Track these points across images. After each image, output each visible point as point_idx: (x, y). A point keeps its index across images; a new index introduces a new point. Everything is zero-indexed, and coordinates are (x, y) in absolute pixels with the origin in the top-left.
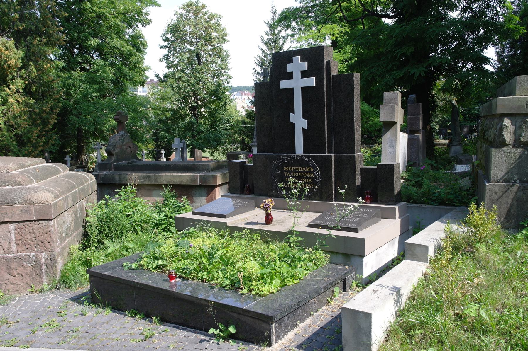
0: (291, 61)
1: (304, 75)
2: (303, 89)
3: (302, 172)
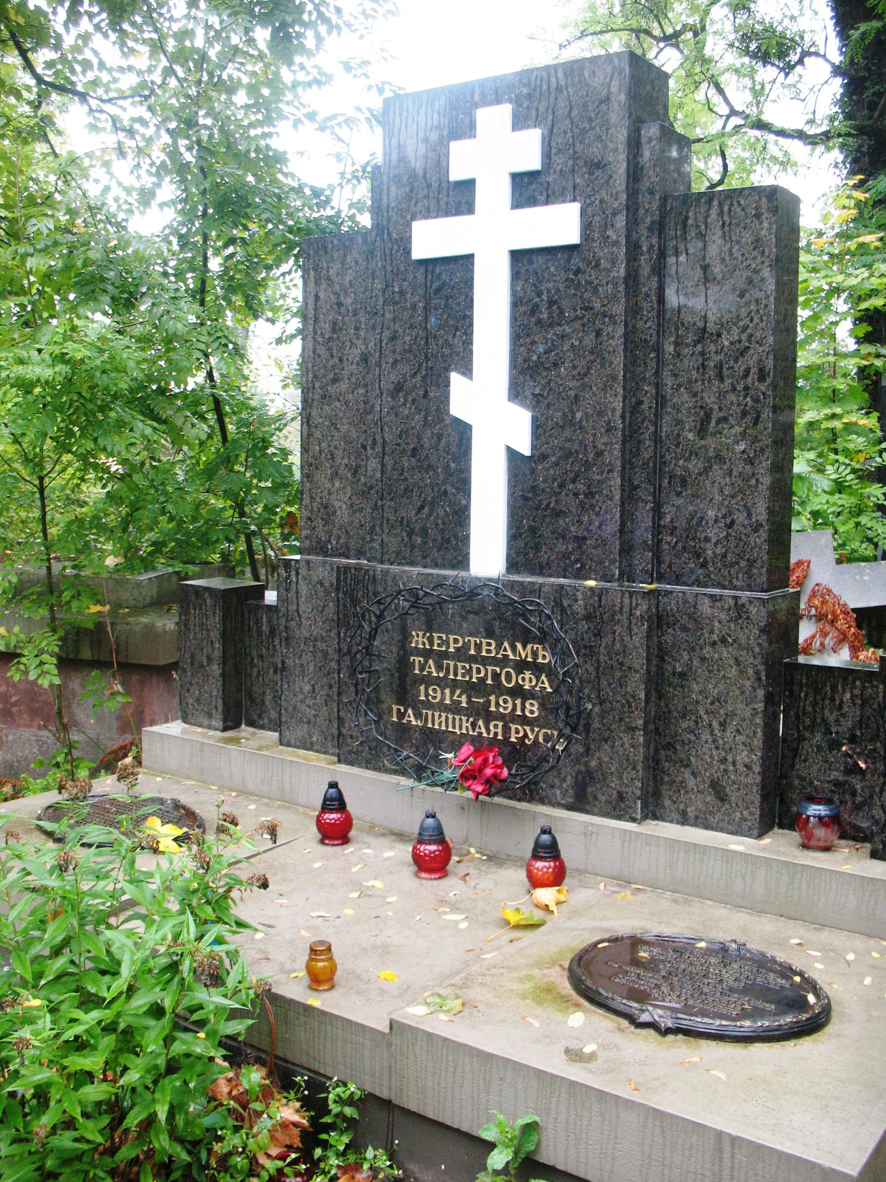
1: (528, 189)
3: (494, 661)
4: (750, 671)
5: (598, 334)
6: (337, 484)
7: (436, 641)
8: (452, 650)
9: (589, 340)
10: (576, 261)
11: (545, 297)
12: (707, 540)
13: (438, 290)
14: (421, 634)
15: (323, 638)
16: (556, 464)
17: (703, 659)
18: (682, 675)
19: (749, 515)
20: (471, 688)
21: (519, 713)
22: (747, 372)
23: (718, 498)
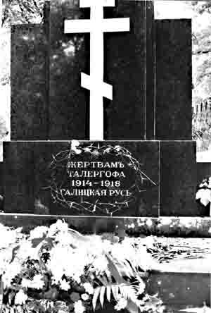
3: (102, 169)
20: (92, 180)
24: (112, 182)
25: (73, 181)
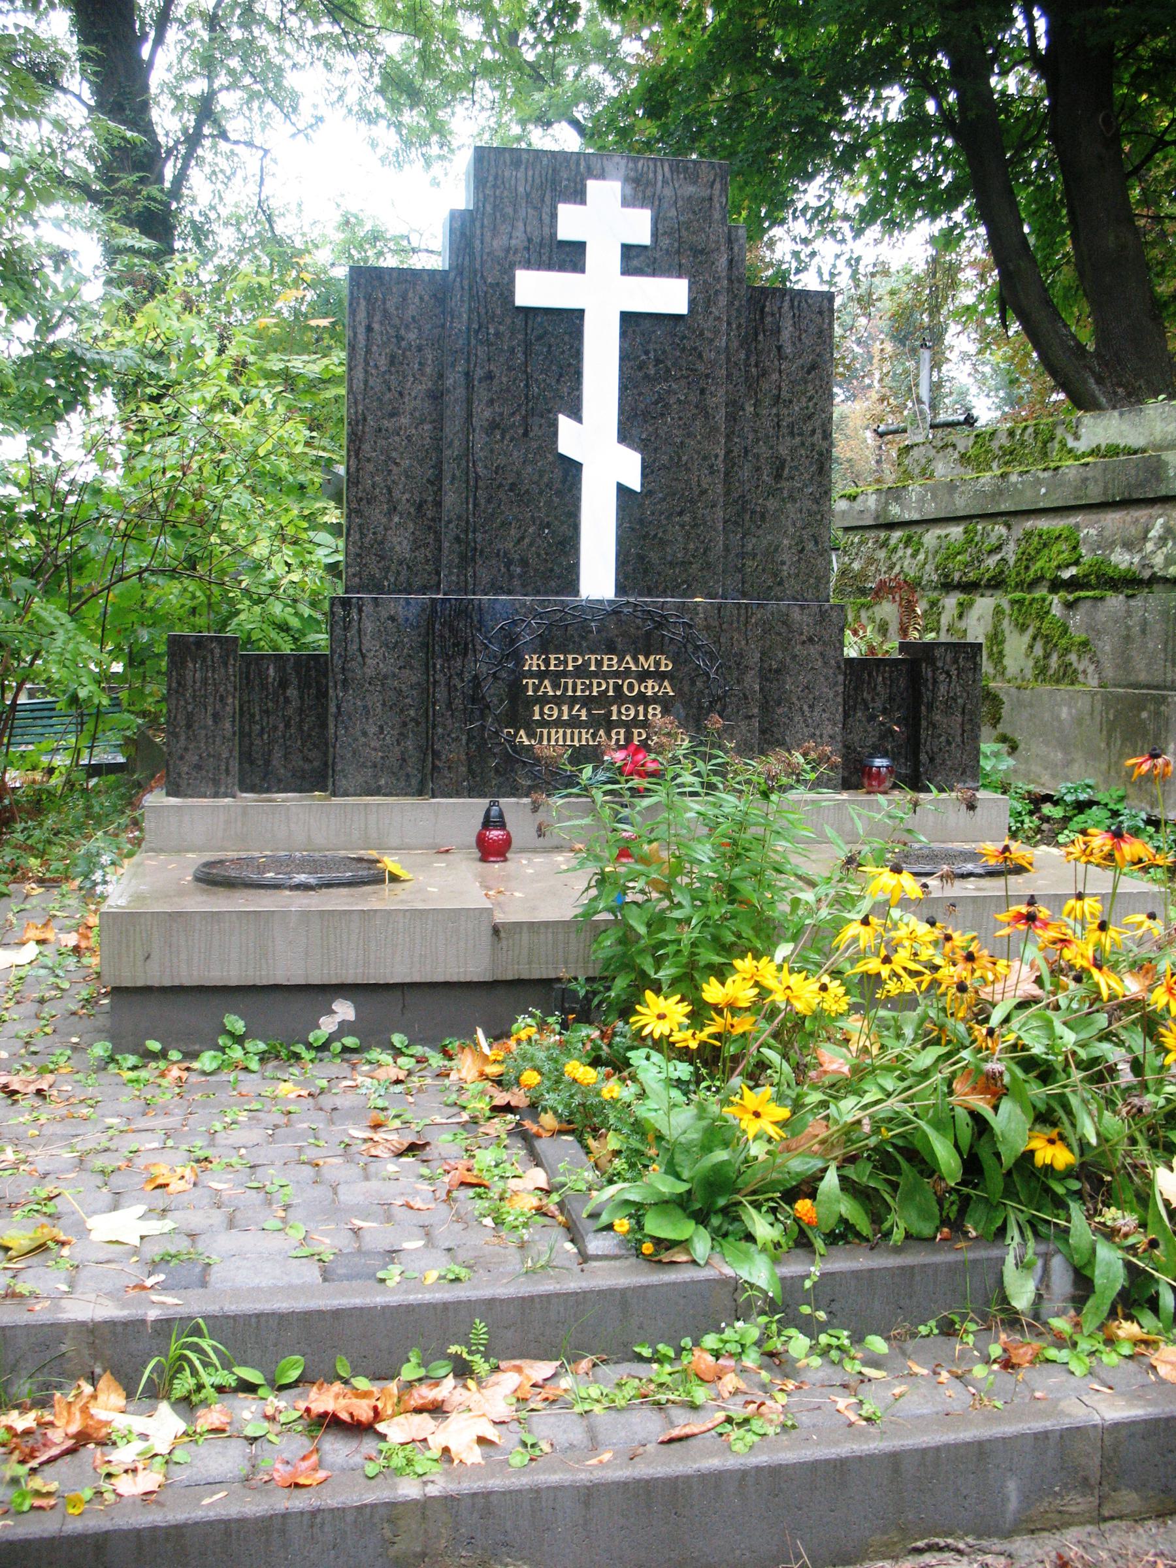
0: (578, 196)
1: (635, 260)
2: (629, 320)
3: (616, 674)
4: (833, 662)
5: (703, 391)
6: (396, 519)
7: (553, 662)
8: (570, 668)
9: (694, 398)
10: (681, 328)
11: (652, 355)
12: (783, 563)
13: (539, 338)
14: (535, 657)
15: (394, 675)
16: (664, 499)
17: (794, 657)
18: (777, 671)
19: (816, 543)
20: (587, 702)
21: (641, 718)
22: (813, 432)
23: (791, 530)
24: (641, 708)
25: (537, 709)
